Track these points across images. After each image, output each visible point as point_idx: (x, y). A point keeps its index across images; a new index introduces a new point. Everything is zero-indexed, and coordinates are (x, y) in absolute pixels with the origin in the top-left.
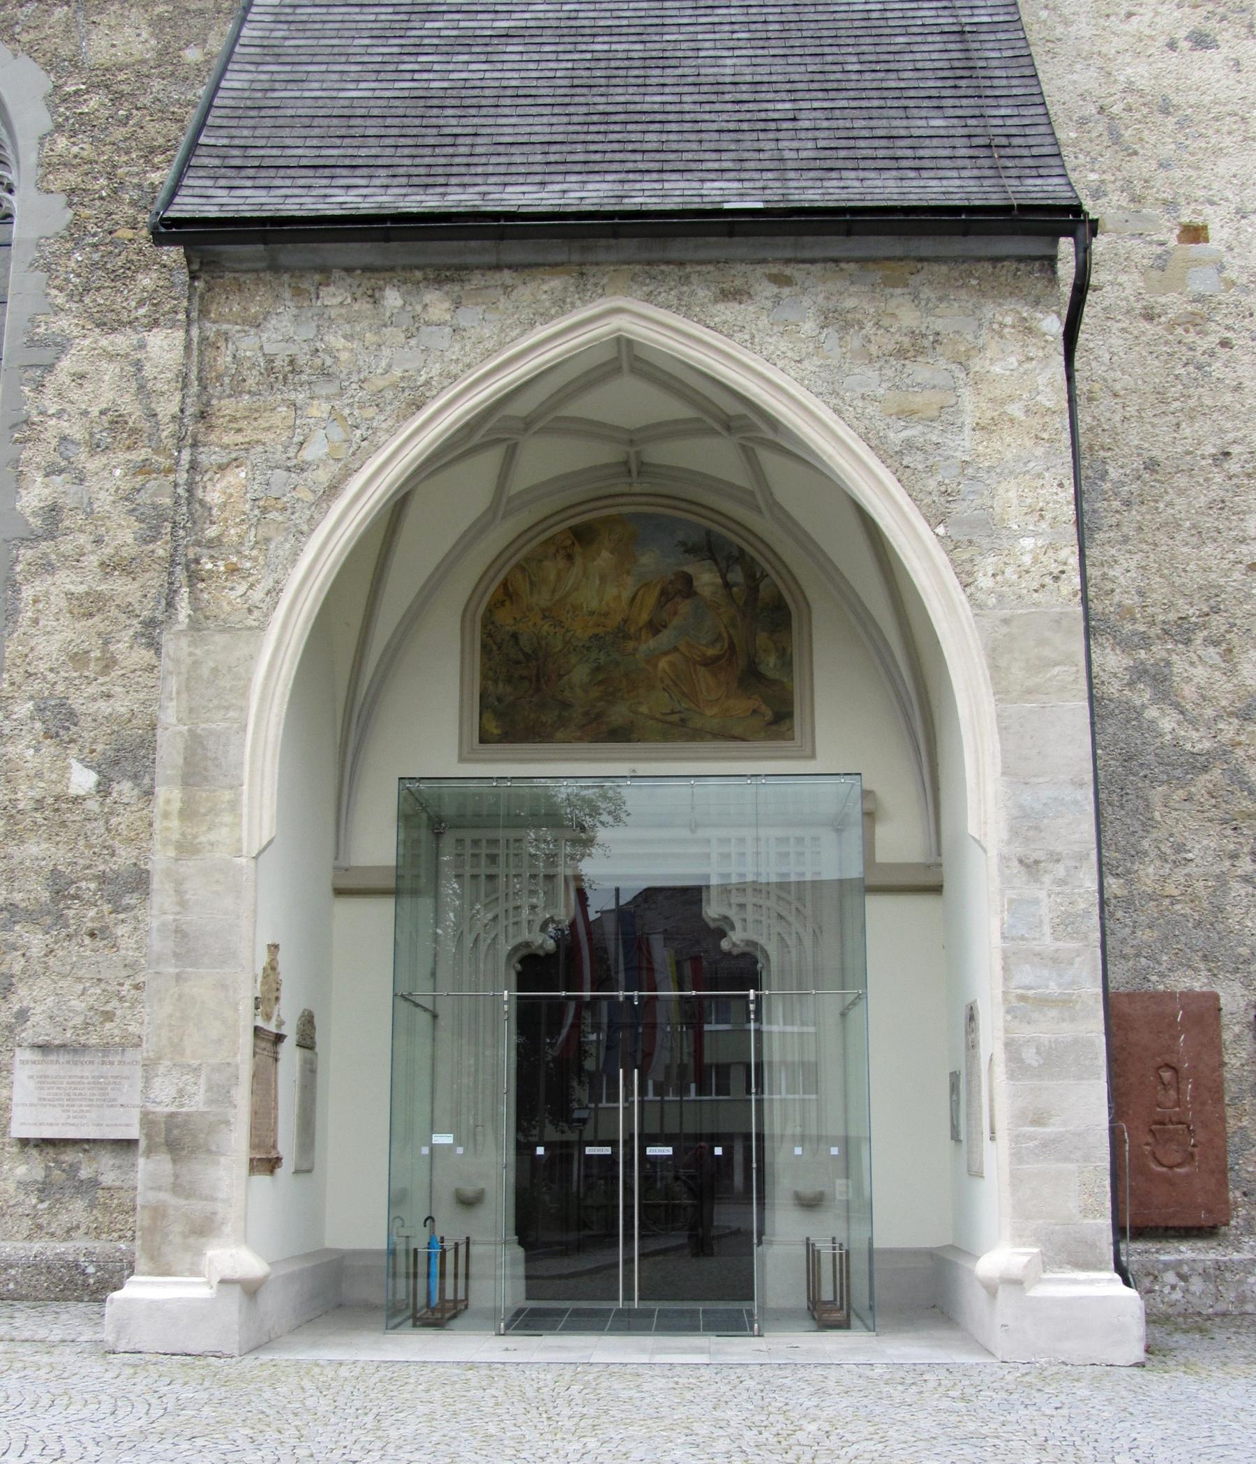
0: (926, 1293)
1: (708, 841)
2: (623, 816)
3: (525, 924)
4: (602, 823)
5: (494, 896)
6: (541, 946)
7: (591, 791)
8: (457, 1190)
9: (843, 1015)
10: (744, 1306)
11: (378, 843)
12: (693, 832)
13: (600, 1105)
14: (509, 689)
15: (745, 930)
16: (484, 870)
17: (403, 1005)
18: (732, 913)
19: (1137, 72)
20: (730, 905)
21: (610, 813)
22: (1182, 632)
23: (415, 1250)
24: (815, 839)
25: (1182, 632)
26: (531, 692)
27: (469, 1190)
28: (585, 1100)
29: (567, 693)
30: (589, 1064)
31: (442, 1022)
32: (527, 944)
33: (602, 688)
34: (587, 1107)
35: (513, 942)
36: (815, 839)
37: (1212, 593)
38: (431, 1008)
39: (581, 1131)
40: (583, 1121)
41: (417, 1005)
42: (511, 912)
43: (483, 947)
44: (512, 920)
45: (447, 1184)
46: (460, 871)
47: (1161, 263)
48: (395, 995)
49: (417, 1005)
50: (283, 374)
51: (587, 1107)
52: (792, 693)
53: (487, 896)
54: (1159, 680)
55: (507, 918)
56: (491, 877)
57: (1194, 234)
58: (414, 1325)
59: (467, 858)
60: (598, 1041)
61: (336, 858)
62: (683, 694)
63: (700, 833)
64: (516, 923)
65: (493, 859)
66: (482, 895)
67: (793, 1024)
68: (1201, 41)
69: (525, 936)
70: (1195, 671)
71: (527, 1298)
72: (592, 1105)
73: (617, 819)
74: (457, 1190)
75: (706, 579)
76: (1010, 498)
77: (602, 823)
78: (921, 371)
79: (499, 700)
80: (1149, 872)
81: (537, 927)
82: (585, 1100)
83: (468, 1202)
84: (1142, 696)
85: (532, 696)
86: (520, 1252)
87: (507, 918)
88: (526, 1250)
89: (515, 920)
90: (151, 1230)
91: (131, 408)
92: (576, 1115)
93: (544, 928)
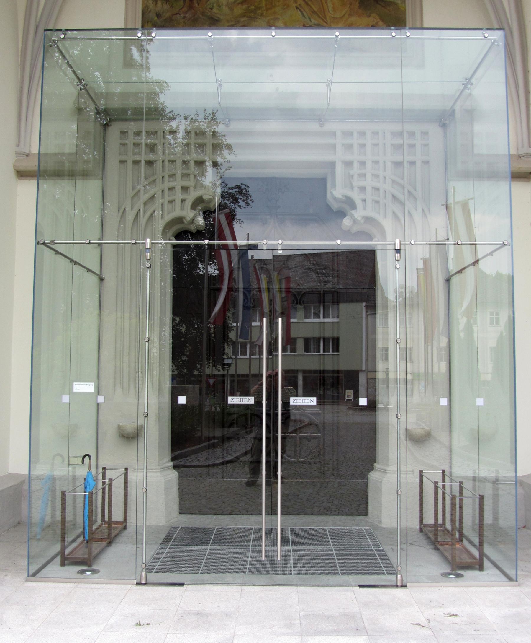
1: (334, 134)
2: (250, 202)
3: (178, 202)
4: (239, 206)
5: (151, 179)
6: (192, 221)
7: (234, 190)
8: (119, 427)
9: (448, 281)
12: (322, 125)
13: (238, 357)
14: (166, 7)
15: (365, 209)
16: (143, 157)
17: (47, 252)
18: (356, 196)
20: (352, 188)
21: (244, 201)
23: (63, 494)
24: (425, 134)
26: (185, 9)
27: (130, 426)
28: (230, 354)
29: (215, 10)
30: (232, 335)
31: (106, 283)
32: (179, 220)
33: (245, 7)
34: (231, 358)
35: (168, 218)
36: (425, 134)
38: (98, 272)
39: (228, 370)
40: (229, 365)
41: (57, 252)
42: (166, 192)
43: (143, 220)
44: (167, 198)
45: (111, 422)
46: (123, 158)
48: (38, 243)
49: (57, 252)
51: (231, 358)
52: (404, 13)
53: (146, 178)
55: (163, 197)
56: (150, 163)
58: (63, 564)
59: (130, 146)
60: (237, 326)
61: (18, 145)
62: (314, 12)
63: (330, 127)
64: (171, 202)
65: (152, 148)
66: (143, 179)
67: (329, 317)
69: (177, 213)
71: (182, 511)
72: (234, 357)
73: (247, 204)
74: (119, 427)
77: (239, 206)
79: (158, 15)
81: (188, 204)
82: (230, 354)
83: (130, 437)
85: (186, 13)
86: (174, 475)
87: (163, 197)
89: (171, 198)
92: (226, 361)
93: (194, 206)
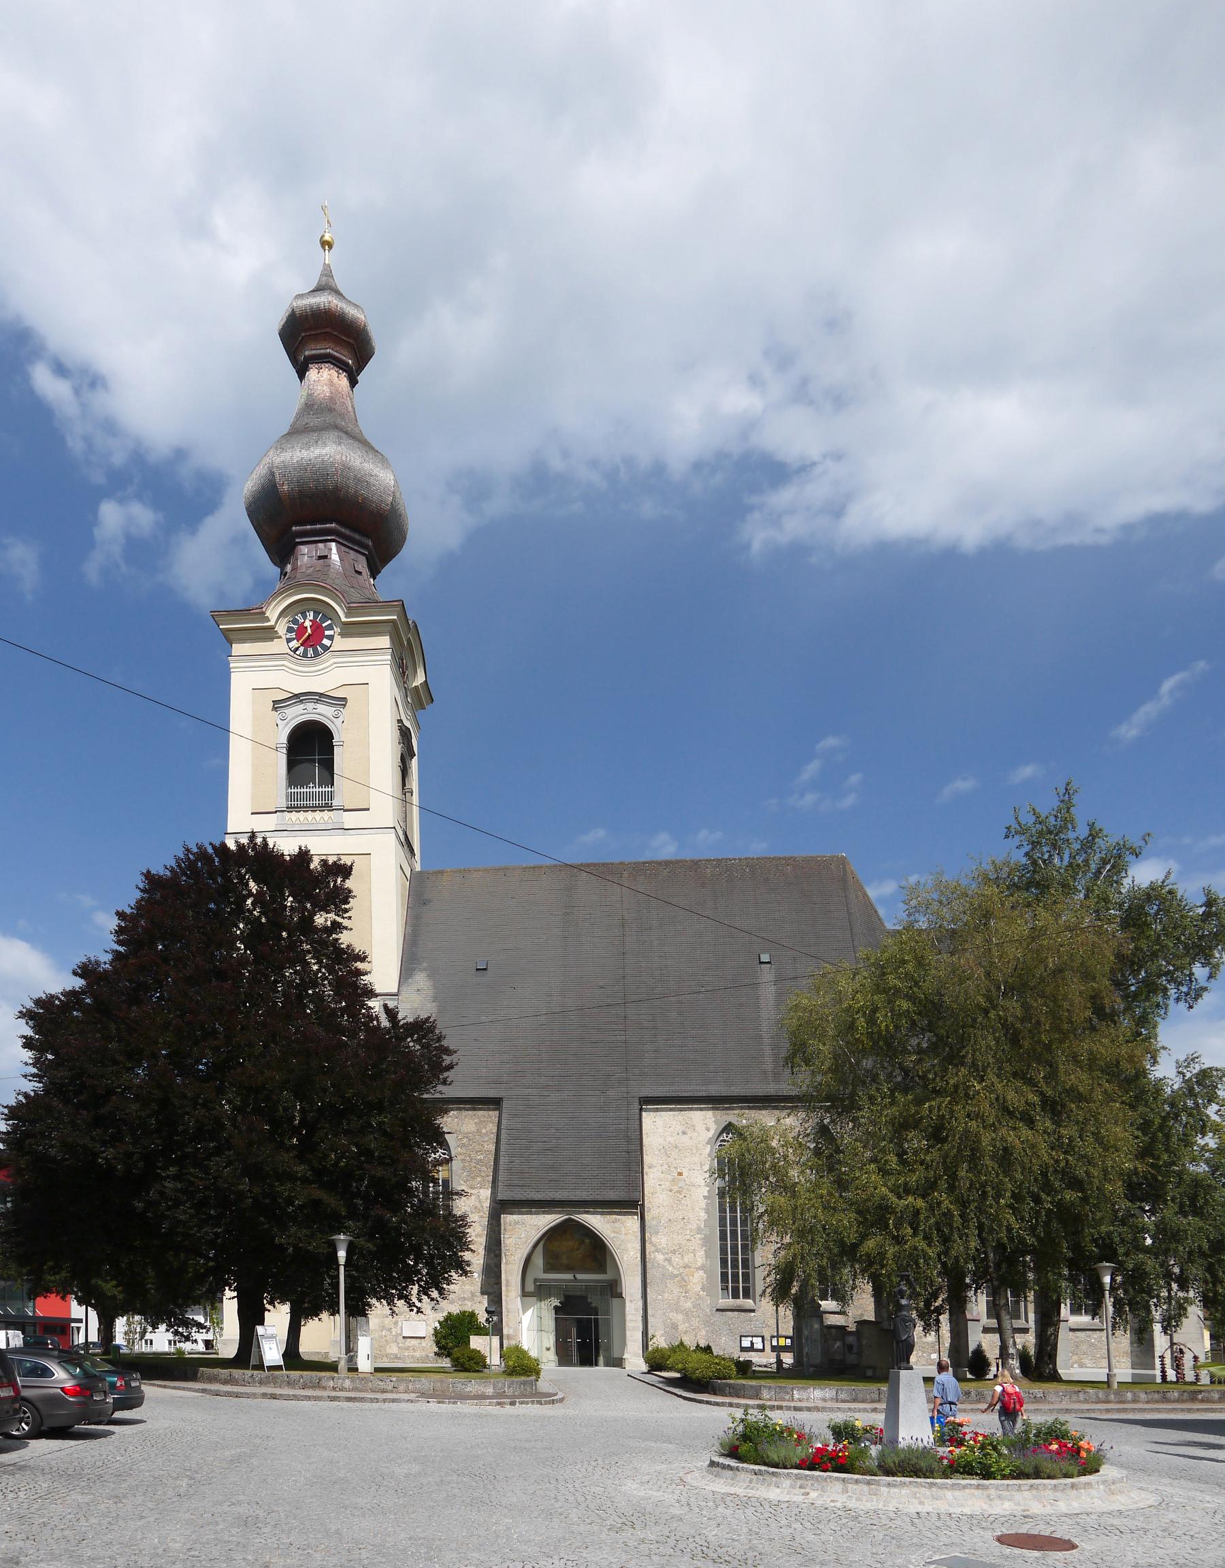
0: (618, 1363)
10: (575, 1359)
11: (530, 1287)
19: (671, 1139)
22: (674, 1252)
25: (674, 1252)
37: (680, 1245)
47: (673, 1180)
50: (517, 1223)
54: (669, 1260)
57: (680, 1174)
68: (684, 1133)
70: (676, 1259)
75: (587, 1241)
76: (630, 1245)
78: (616, 1225)
80: (666, 1295)
84: (666, 1264)
88: (31, 392)
90: (1122, 1306)
91: (478, 1204)
